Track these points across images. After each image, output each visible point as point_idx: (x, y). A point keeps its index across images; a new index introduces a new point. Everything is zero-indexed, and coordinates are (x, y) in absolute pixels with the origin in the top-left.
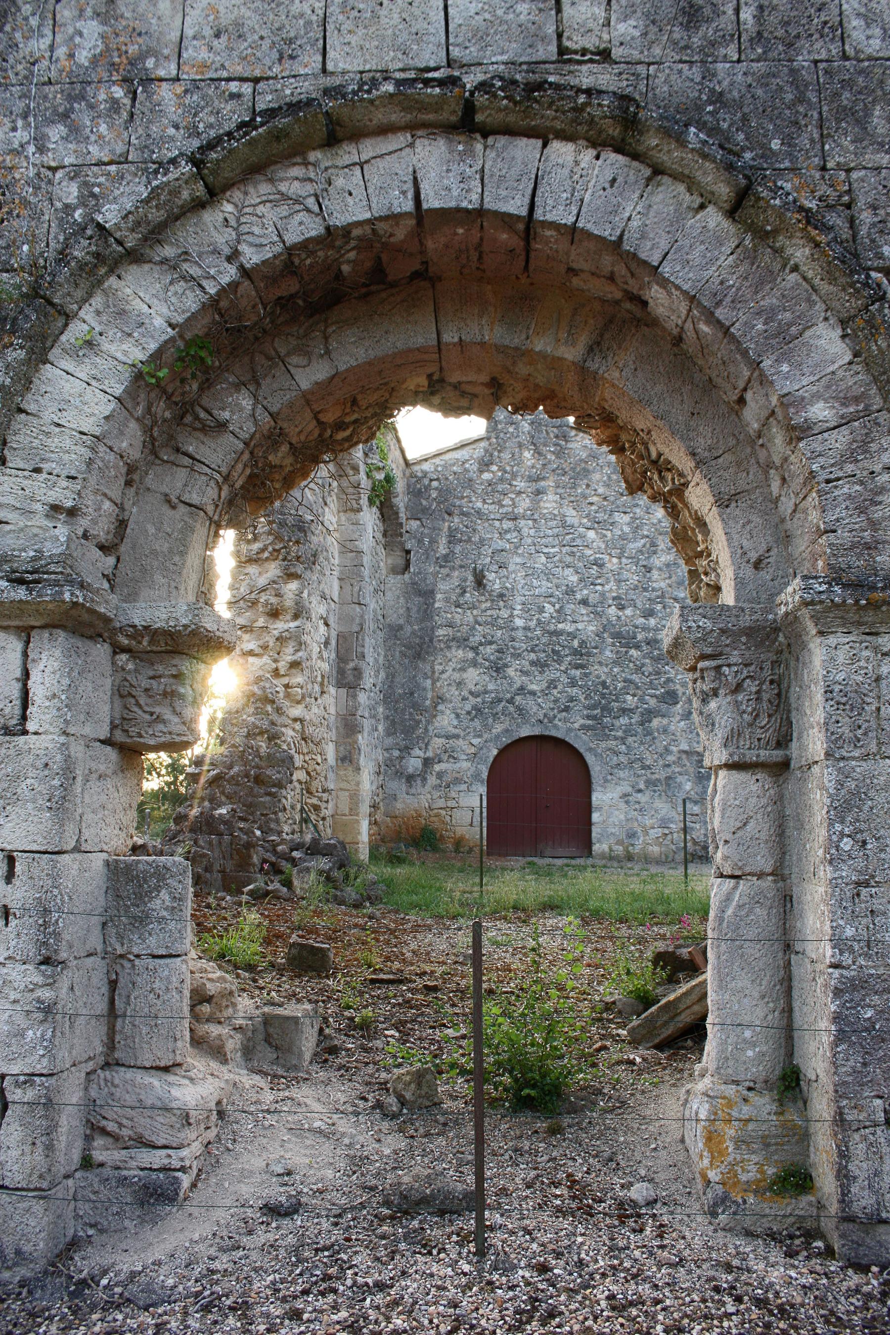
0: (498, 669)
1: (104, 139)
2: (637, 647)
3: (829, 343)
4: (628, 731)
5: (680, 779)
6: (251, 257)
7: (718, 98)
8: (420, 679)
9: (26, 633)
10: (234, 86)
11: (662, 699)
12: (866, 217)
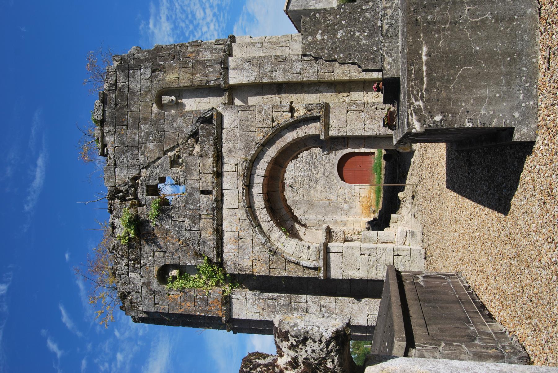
0: (317, 181)
7: (244, 148)
8: (320, 204)
10: (240, 223)
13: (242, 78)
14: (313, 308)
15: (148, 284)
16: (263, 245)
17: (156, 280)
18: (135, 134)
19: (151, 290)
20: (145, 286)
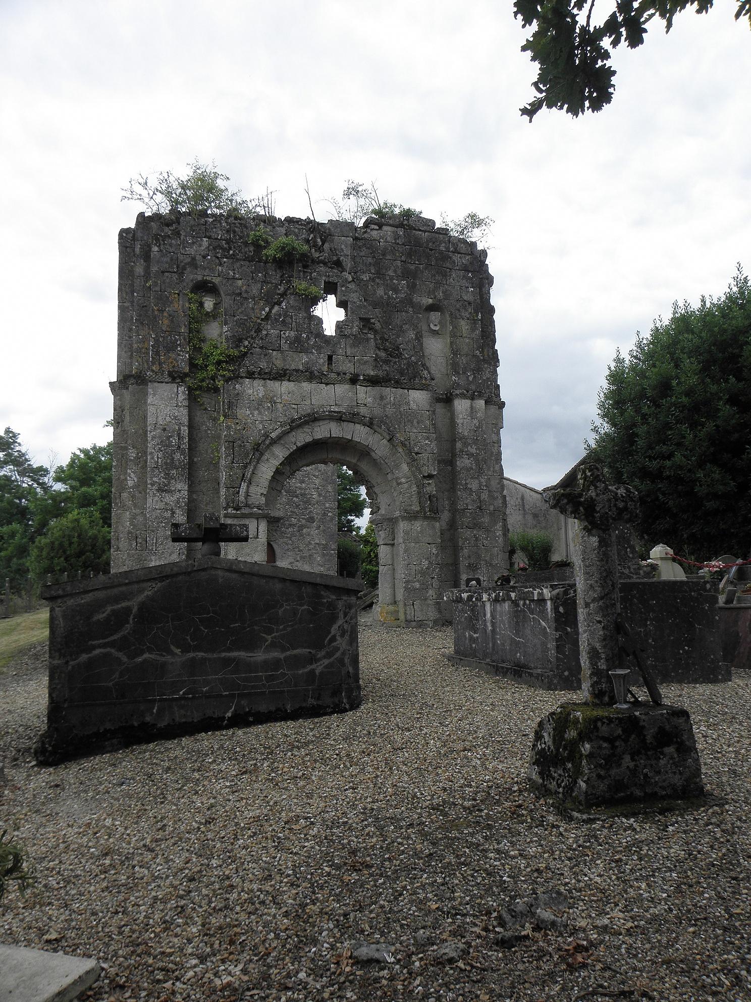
1: (266, 415)
2: (297, 497)
3: (405, 467)
4: (293, 535)
5: (315, 556)
6: (299, 444)
7: (386, 416)
9: (257, 519)
11: (308, 520)
12: (412, 443)
13: (461, 416)
14: (170, 499)
15: (193, 263)
16: (266, 436)
17: (200, 278)
18: (395, 271)
19: (184, 268)
20: (189, 260)
